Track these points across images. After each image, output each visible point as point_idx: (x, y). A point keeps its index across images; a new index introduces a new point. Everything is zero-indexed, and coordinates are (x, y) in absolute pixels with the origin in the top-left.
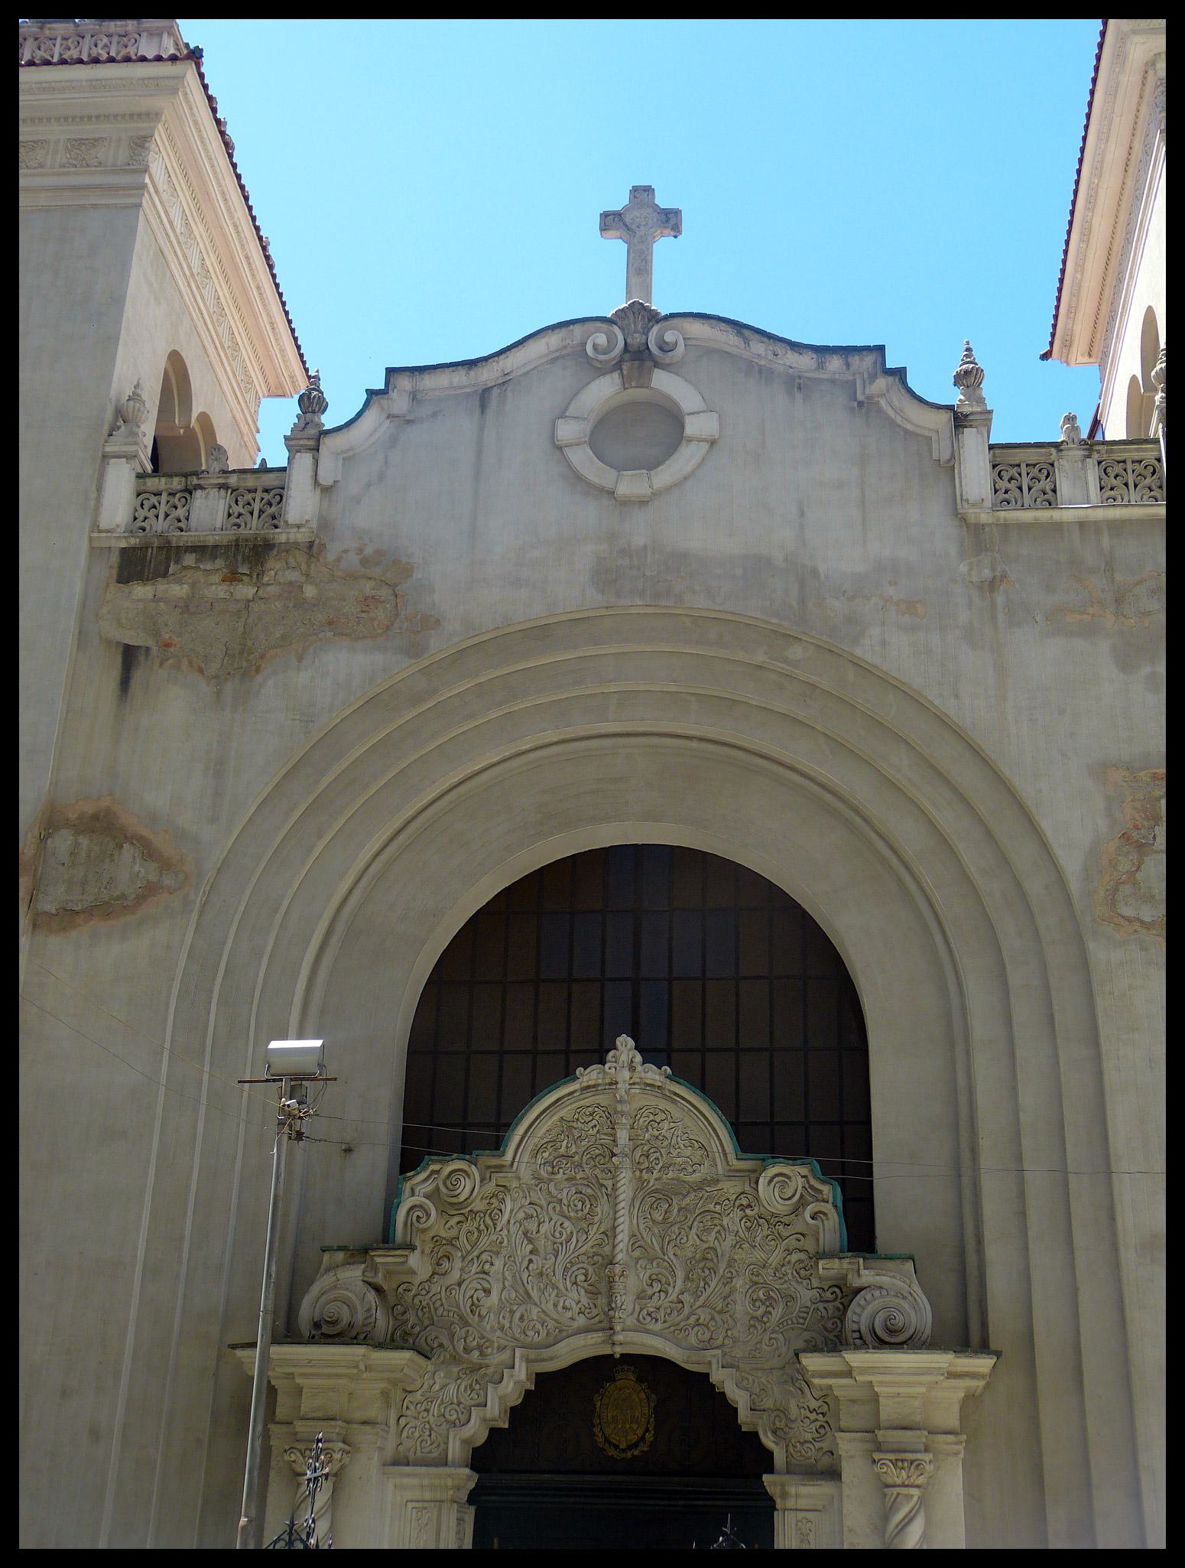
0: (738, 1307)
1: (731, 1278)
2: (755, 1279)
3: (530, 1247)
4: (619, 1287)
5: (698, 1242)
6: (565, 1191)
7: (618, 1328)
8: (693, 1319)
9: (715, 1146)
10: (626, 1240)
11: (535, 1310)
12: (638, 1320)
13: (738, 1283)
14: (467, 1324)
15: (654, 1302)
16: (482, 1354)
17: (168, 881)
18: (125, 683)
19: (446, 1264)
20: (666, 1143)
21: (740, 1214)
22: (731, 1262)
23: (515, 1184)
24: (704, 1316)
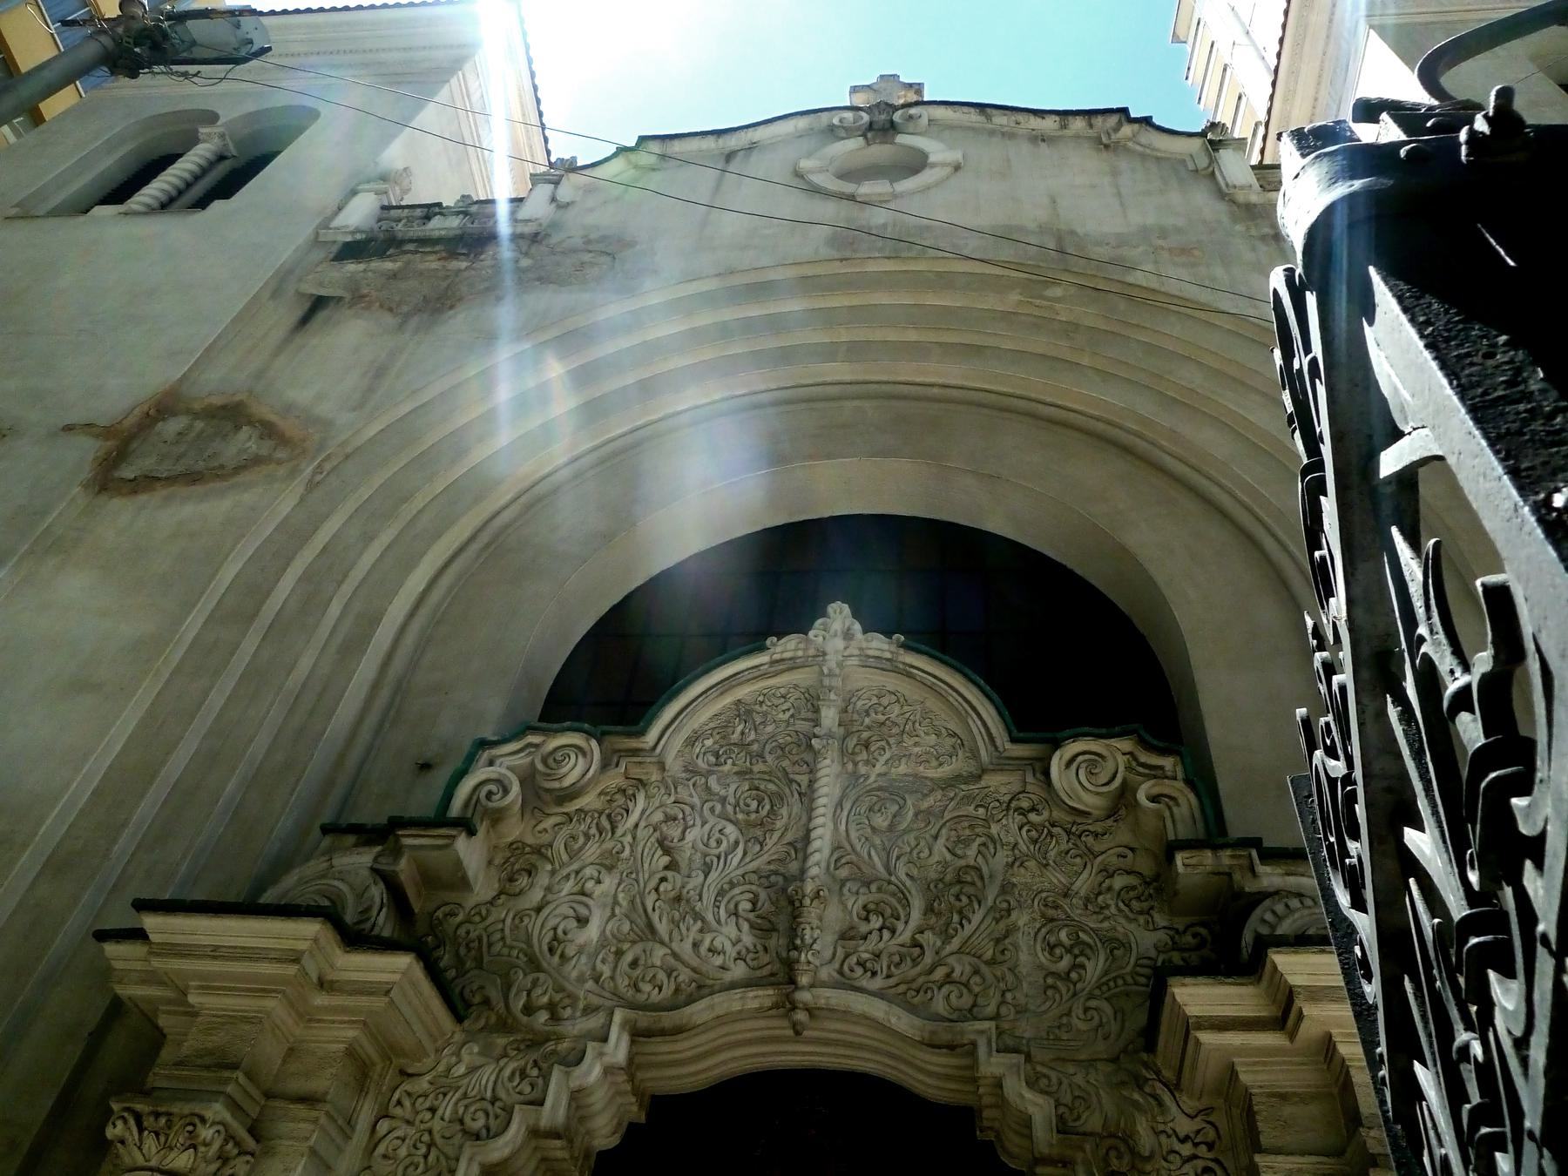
0: (1024, 957)
1: (1009, 911)
2: (1051, 912)
3: (666, 859)
4: (811, 913)
5: (948, 856)
6: (733, 787)
7: (804, 980)
8: (940, 973)
9: (975, 726)
10: (826, 852)
11: (660, 952)
12: (840, 972)
13: (1021, 918)
14: (539, 969)
15: (872, 943)
16: (555, 1017)
17: (281, 454)
18: (305, 320)
19: (523, 881)
20: (895, 730)
21: (1019, 818)
22: (1007, 887)
23: (655, 776)
24: (961, 968)
